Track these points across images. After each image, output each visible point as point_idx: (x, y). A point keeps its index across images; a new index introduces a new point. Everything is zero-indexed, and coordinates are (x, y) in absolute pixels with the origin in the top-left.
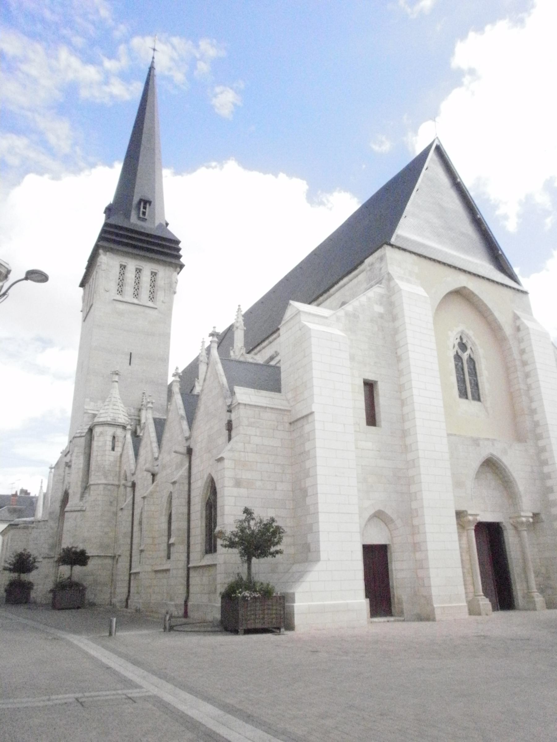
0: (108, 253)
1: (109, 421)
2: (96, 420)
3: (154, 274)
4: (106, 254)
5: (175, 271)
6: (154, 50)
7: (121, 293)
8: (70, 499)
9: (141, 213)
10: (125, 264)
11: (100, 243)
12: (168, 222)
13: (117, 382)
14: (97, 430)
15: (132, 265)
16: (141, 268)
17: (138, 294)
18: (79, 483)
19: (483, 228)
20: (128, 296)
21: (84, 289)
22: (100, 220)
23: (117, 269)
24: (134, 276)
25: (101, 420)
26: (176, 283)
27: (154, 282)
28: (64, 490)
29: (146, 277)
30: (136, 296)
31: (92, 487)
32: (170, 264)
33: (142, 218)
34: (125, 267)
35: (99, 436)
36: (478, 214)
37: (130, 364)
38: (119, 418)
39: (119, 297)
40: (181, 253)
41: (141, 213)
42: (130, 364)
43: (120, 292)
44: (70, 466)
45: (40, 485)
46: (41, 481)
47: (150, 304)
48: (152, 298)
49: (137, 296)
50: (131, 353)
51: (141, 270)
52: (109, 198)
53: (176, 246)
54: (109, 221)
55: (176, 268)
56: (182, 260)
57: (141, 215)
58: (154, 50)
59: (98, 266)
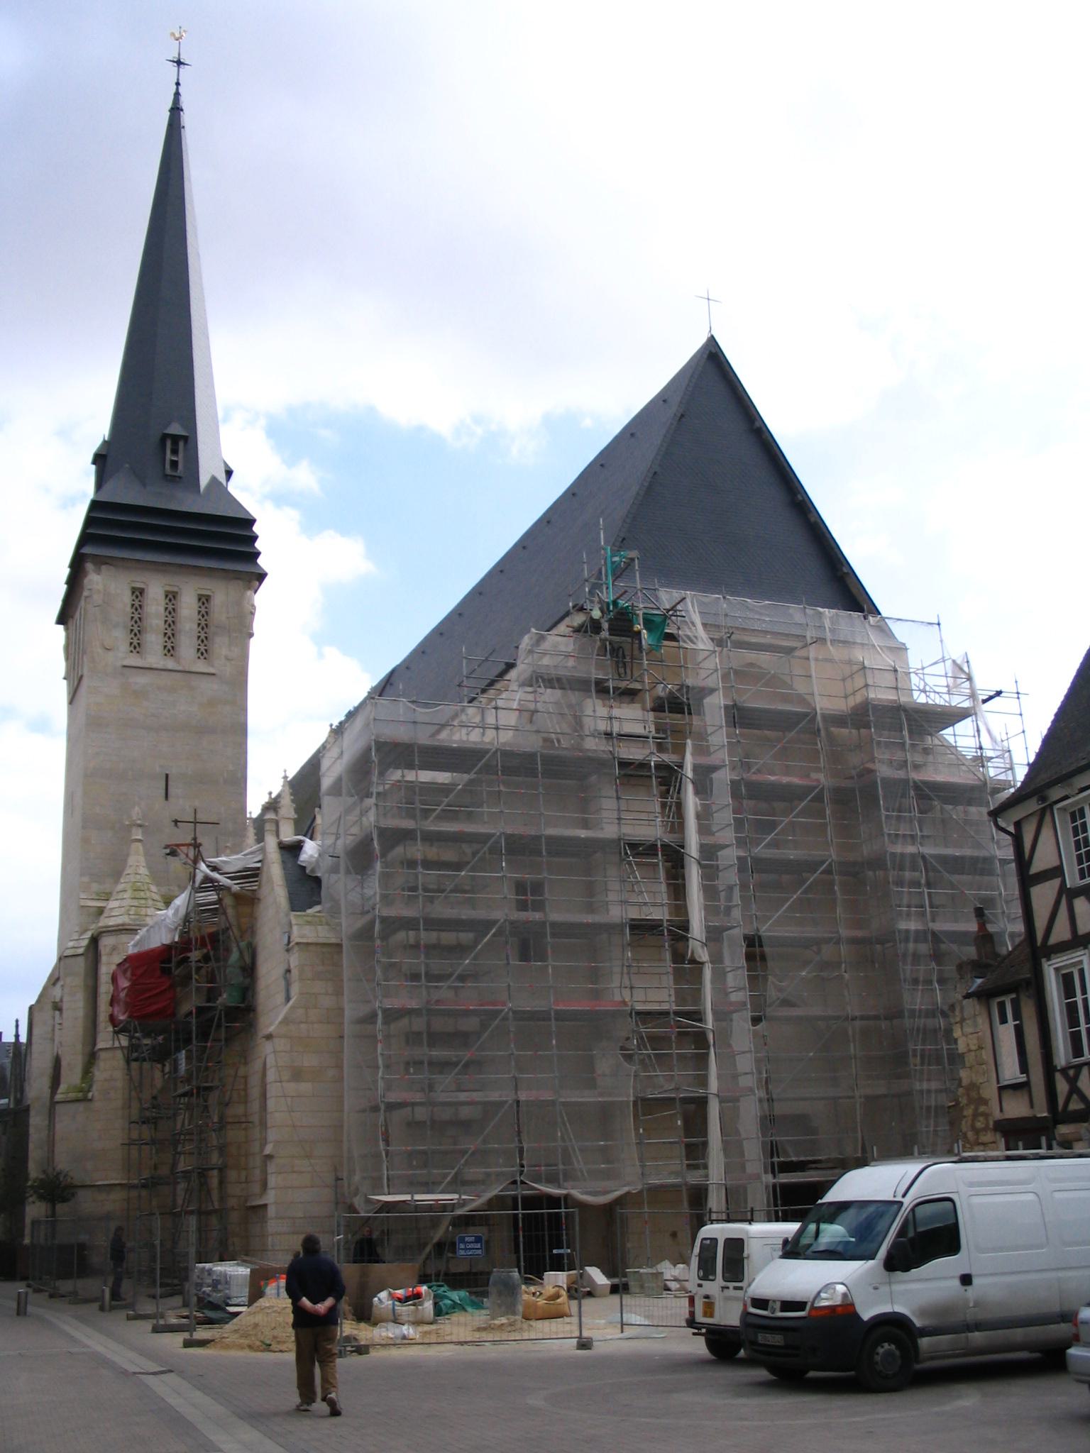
0: (104, 567)
1: (129, 925)
2: (105, 922)
3: (204, 600)
4: (100, 569)
5: (249, 589)
6: (179, 63)
7: (138, 649)
8: (63, 1079)
9: (168, 466)
10: (142, 586)
11: (87, 550)
12: (232, 466)
13: (139, 841)
14: (106, 942)
15: (156, 589)
16: (175, 589)
17: (173, 635)
18: (79, 1047)
19: (812, 520)
20: (154, 656)
21: (67, 629)
22: (84, 486)
23: (127, 598)
24: (162, 609)
25: (112, 922)
26: (253, 614)
27: (206, 617)
28: (55, 1054)
29: (188, 606)
30: (169, 651)
31: (103, 1055)
32: (237, 576)
33: (171, 476)
34: (142, 591)
35: (110, 954)
36: (799, 493)
37: (167, 797)
38: (146, 915)
39: (134, 660)
40: (259, 545)
41: (168, 466)
42: (167, 797)
43: (136, 647)
44: (60, 1010)
45: (14, 1033)
46: (14, 1023)
47: (201, 666)
48: (204, 652)
49: (172, 651)
50: (167, 776)
51: (177, 593)
52: (99, 427)
53: (248, 534)
54: (105, 497)
55: (250, 582)
56: (260, 561)
57: (168, 471)
58: (179, 63)
59: (86, 597)
